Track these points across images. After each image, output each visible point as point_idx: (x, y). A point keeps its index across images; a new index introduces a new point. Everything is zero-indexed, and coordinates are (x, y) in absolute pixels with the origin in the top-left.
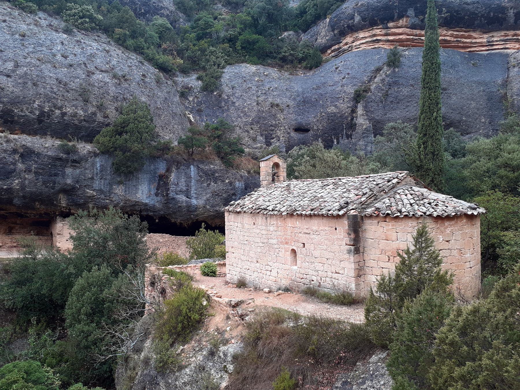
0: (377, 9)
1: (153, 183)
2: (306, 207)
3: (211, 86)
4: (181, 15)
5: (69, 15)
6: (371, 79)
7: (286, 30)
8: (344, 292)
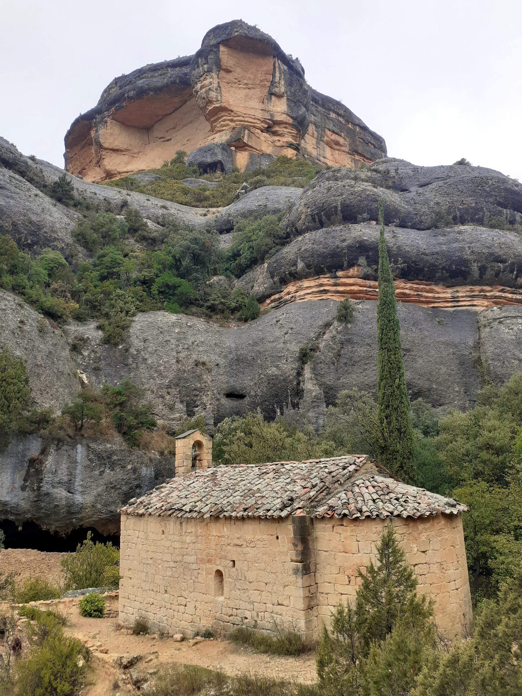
0: (323, 256)
1: (19, 471)
2: (238, 505)
4: (80, 249)
6: (320, 335)
7: (215, 274)
8: (290, 633)
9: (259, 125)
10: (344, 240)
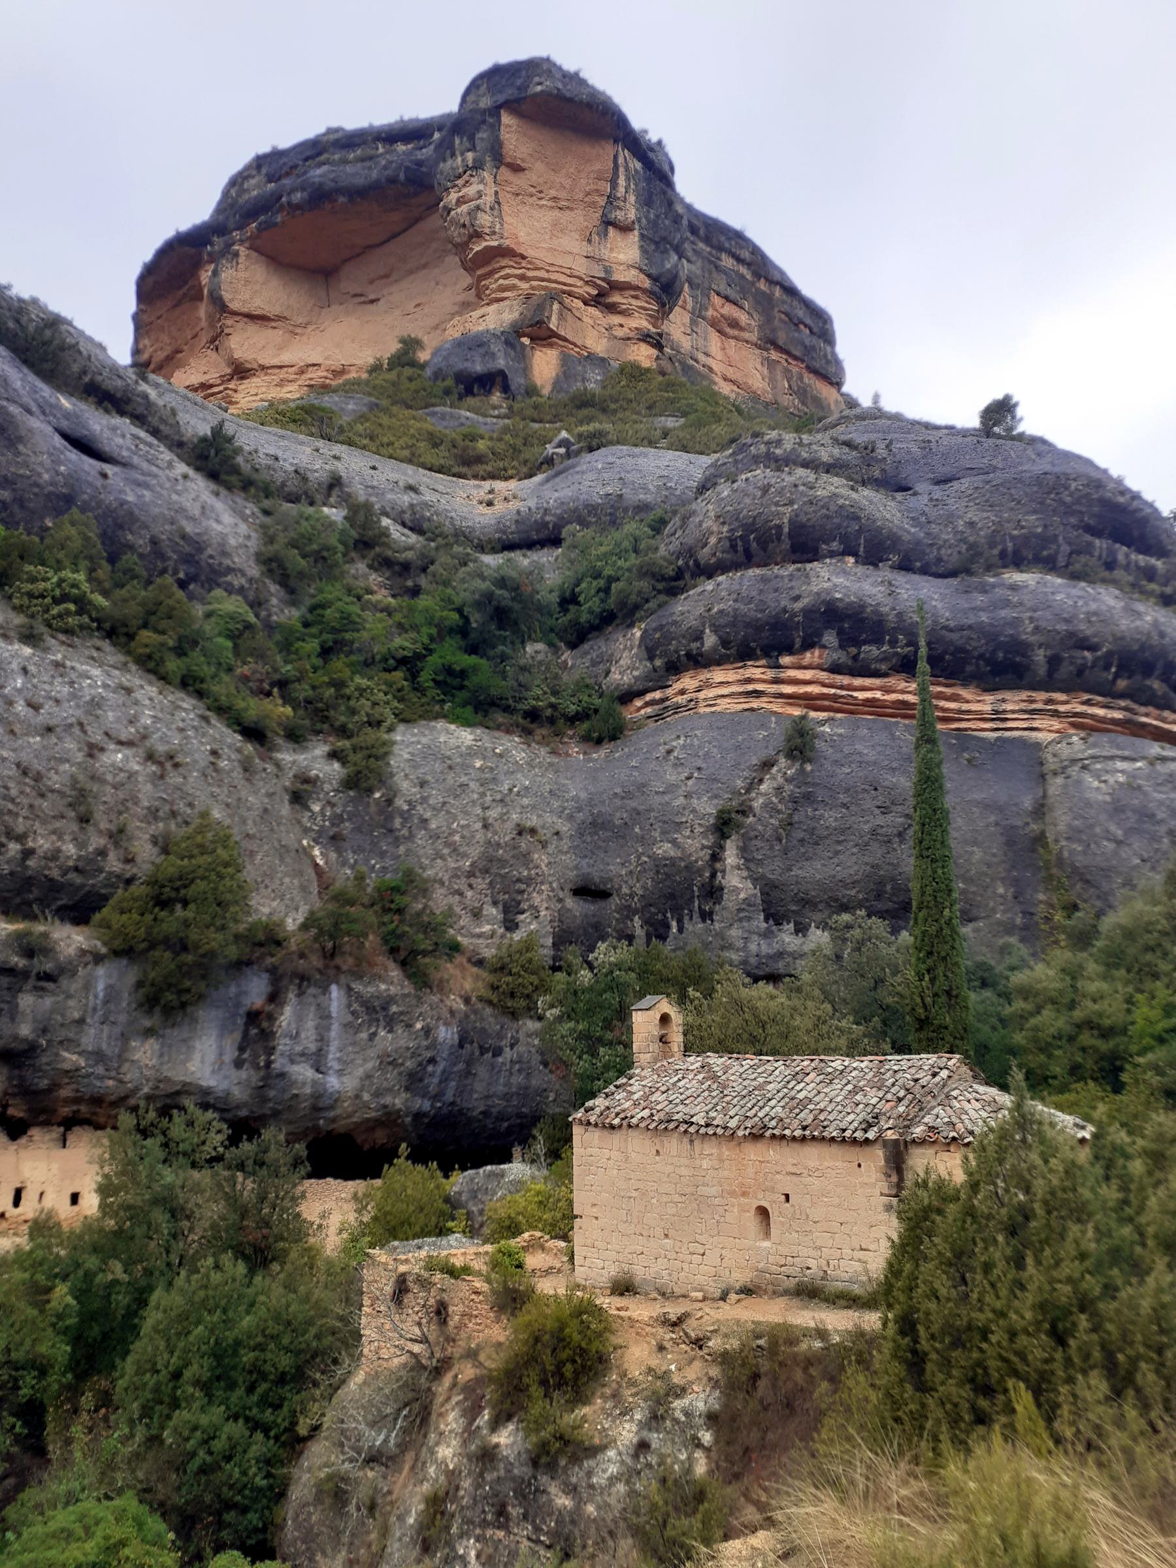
0: (756, 626)
1: (232, 1031)
3: (365, 776)
4: (274, 588)
5: (31, 595)
9: (580, 291)
10: (797, 598)
